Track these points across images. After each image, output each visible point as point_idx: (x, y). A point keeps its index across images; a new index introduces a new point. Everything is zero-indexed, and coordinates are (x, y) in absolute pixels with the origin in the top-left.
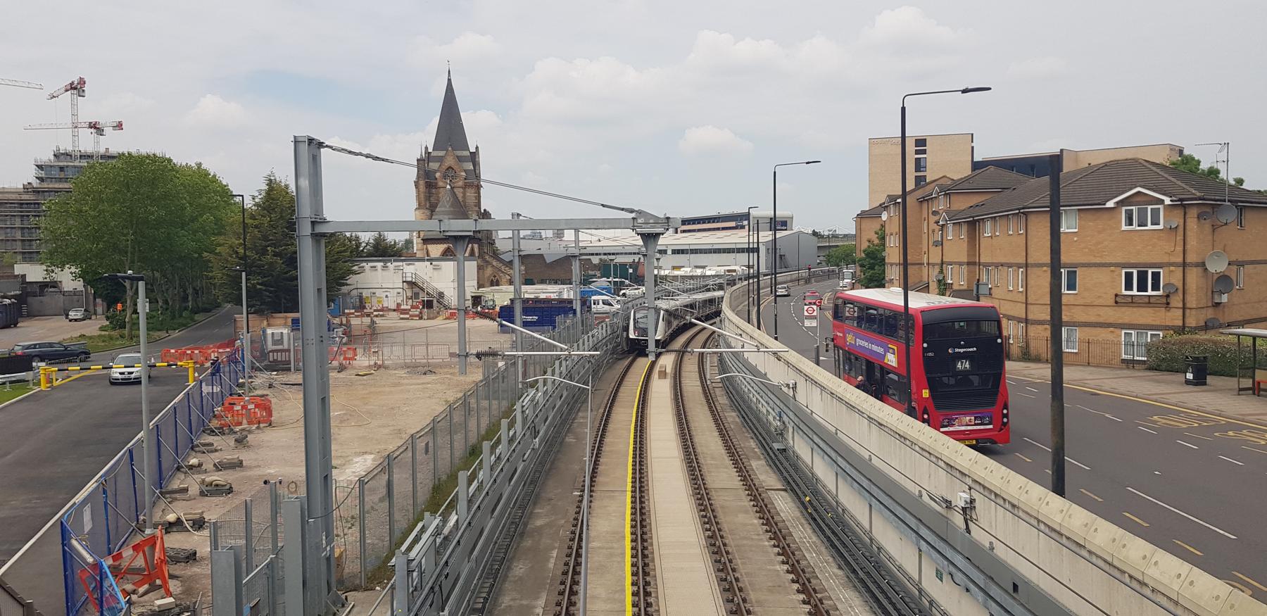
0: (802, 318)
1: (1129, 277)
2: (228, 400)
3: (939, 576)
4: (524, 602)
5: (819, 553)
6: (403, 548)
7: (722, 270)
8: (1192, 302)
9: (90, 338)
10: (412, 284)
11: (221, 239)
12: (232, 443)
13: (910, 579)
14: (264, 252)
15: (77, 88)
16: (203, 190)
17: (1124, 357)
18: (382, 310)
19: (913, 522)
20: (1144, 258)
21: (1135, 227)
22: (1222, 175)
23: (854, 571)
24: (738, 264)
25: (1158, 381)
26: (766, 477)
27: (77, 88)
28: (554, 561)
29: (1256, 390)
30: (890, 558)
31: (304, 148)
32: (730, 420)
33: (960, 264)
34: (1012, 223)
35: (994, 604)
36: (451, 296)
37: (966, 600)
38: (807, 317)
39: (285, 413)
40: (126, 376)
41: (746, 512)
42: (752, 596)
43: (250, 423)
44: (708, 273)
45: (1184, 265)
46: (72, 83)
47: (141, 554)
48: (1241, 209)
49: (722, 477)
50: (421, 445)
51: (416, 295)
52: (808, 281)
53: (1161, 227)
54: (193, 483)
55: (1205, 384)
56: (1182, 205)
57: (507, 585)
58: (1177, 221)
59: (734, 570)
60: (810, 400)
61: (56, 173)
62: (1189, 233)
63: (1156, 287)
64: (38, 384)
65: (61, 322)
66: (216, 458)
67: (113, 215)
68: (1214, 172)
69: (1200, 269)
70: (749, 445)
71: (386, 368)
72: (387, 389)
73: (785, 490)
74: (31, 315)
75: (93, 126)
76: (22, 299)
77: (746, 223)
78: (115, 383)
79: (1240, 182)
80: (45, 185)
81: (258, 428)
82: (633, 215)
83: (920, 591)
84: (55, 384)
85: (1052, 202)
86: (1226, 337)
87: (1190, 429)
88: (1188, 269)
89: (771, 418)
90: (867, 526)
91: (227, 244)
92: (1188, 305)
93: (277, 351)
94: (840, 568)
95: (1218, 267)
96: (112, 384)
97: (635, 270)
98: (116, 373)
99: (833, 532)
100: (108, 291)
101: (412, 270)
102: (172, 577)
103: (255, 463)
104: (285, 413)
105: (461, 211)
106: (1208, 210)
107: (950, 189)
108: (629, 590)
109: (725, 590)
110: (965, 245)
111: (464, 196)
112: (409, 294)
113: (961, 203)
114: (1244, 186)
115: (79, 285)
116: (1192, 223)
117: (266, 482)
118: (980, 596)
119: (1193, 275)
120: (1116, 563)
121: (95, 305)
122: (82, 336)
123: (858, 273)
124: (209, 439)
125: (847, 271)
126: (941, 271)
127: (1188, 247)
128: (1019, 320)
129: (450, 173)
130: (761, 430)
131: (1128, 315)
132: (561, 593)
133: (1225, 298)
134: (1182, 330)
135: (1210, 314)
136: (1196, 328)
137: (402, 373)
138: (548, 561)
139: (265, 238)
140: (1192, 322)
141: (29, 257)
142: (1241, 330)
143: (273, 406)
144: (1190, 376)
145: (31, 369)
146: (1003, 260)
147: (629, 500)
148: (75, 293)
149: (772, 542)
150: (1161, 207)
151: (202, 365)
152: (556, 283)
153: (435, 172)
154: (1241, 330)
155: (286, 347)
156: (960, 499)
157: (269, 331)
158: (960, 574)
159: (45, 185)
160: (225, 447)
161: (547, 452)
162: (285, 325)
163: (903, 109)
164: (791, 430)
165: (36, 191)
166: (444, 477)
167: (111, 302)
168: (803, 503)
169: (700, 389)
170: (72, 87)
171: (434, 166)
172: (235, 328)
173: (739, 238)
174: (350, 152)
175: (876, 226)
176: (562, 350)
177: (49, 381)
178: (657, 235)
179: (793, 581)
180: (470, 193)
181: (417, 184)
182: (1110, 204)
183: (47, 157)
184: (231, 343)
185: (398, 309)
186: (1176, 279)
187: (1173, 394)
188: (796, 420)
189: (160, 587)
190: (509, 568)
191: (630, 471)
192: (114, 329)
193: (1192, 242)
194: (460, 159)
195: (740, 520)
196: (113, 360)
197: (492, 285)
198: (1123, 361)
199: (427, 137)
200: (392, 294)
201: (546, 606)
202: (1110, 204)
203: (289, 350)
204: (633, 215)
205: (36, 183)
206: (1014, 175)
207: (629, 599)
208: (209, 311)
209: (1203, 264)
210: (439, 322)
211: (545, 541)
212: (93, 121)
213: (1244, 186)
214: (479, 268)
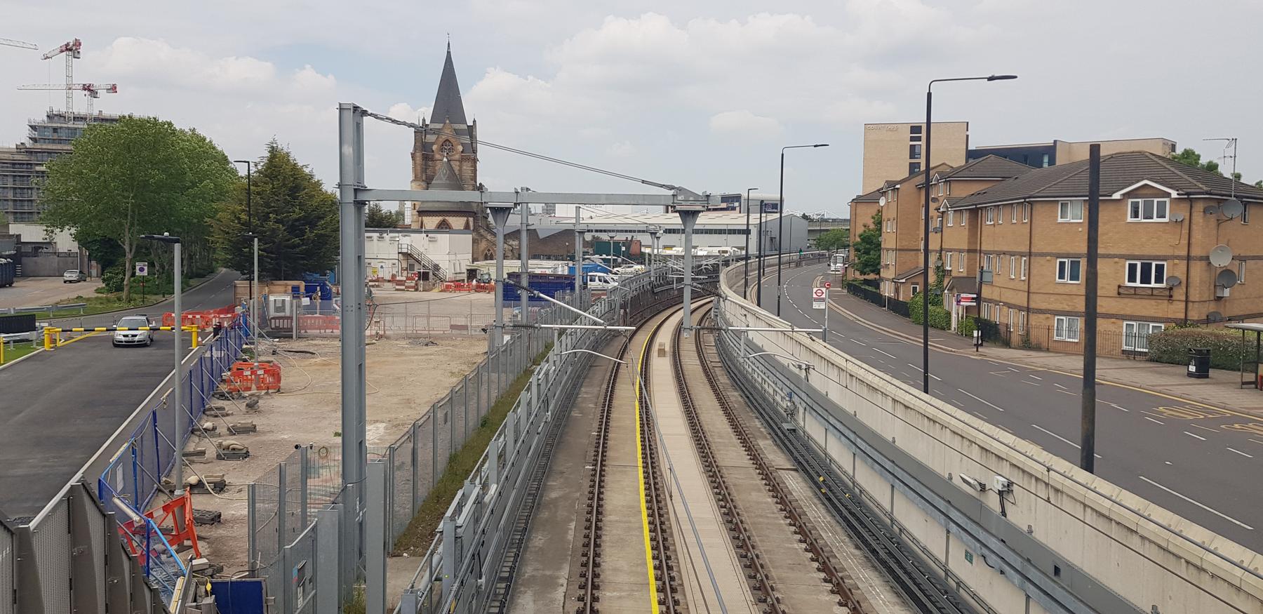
0: (811, 301)
1: (1132, 268)
2: (238, 364)
3: (969, 557)
4: (548, 573)
5: (835, 533)
6: (449, 513)
7: (715, 251)
8: (1195, 295)
9: (88, 299)
10: (408, 256)
11: (221, 205)
12: (243, 407)
13: (936, 560)
14: (266, 218)
15: (72, 49)
16: (202, 157)
17: (1125, 348)
18: (377, 280)
19: (942, 505)
20: (1147, 251)
21: (1141, 219)
22: (1220, 169)
23: (874, 551)
24: (730, 246)
25: (1160, 373)
26: (775, 457)
27: (72, 49)
28: (573, 532)
29: (1262, 384)
30: (914, 539)
31: (349, 115)
32: (733, 399)
33: (960, 251)
34: (1017, 211)
35: (1032, 587)
36: (447, 270)
37: (998, 580)
38: (816, 300)
39: (291, 379)
40: (130, 339)
41: (759, 490)
42: (774, 573)
43: (259, 388)
44: (700, 253)
45: (1188, 258)
46: (67, 45)
47: (171, 515)
48: (1245, 204)
49: (731, 455)
50: (440, 415)
51: (411, 267)
52: (798, 264)
53: (1166, 220)
54: (210, 447)
55: (1207, 377)
56: (1188, 199)
57: (528, 555)
58: (1183, 214)
59: (753, 547)
60: (825, 383)
61: (49, 134)
62: (1194, 227)
63: (1159, 279)
64: (42, 343)
65: (57, 283)
66: (230, 421)
67: (115, 177)
68: (1212, 167)
69: (1204, 263)
70: (755, 424)
71: (388, 338)
72: (391, 359)
73: (796, 470)
74: (25, 275)
75: (87, 88)
76: (17, 258)
77: (736, 204)
78: (118, 345)
79: (1238, 176)
80: (38, 146)
81: (267, 393)
82: (672, 192)
83: (947, 572)
84: (59, 344)
85: (1091, 192)
86: (1230, 332)
87: (1197, 421)
88: (1192, 263)
89: (778, 398)
90: (888, 508)
91: (227, 212)
92: (1191, 298)
93: (279, 318)
94: (857, 547)
95: (1222, 261)
96: (116, 346)
97: (628, 248)
98: (119, 335)
99: (851, 513)
100: (103, 253)
101: (408, 242)
102: (200, 538)
103: (268, 429)
104: (291, 379)
105: (457, 182)
106: (1215, 204)
107: (950, 177)
108: (651, 564)
109: (746, 566)
110: (966, 232)
111: (460, 170)
112: (405, 265)
113: (962, 191)
114: (1242, 181)
115: (74, 247)
116: (1198, 217)
117: (297, 447)
118: (1017, 578)
119: (1197, 269)
120: (1171, 548)
121: (90, 267)
122: (79, 298)
123: (852, 257)
124: (220, 403)
125: (841, 255)
126: (940, 258)
127: (1193, 240)
128: (1020, 309)
129: (447, 145)
130: (767, 409)
131: (1130, 306)
132: (585, 565)
133: (1227, 293)
134: (1184, 323)
135: (1212, 307)
136: (1198, 321)
137: (403, 343)
138: (567, 533)
139: (267, 205)
140: (1194, 315)
141: (21, 217)
142: (1241, 325)
143: (282, 373)
144: (1192, 368)
145: (34, 329)
146: (1005, 249)
147: (641, 475)
148: (69, 254)
149: (788, 521)
150: (1167, 200)
151: (203, 329)
152: (549, 258)
153: (433, 144)
154: (1241, 325)
155: (288, 314)
156: (997, 483)
157: (272, 298)
158: (993, 556)
159: (38, 146)
160: (236, 412)
161: (557, 426)
162: (285, 292)
163: (929, 95)
164: (801, 410)
165: (30, 152)
166: (460, 447)
167: (106, 264)
168: (816, 483)
169: (700, 368)
170: (67, 48)
171: (431, 138)
172: (235, 294)
173: (735, 219)
174: (394, 121)
175: (872, 210)
176: (595, 323)
177: (53, 341)
178: (695, 214)
179: (812, 560)
180: (467, 167)
181: (413, 156)
182: (1117, 196)
183: (41, 118)
184: (231, 309)
185: (393, 280)
186: (1180, 272)
187: (1173, 384)
188: (809, 401)
189: (190, 547)
190: (529, 539)
191: (639, 447)
192: (110, 291)
193: (1197, 236)
194: (458, 132)
195: (754, 499)
196: (115, 322)
197: (486, 258)
198: (1124, 352)
199: (424, 112)
200: (387, 264)
201: (570, 576)
202: (1117, 196)
203: (291, 318)
204: (672, 192)
205: (29, 144)
206: (1015, 165)
207: (651, 573)
208: (204, 276)
209: (1207, 258)
210: (434, 294)
211: (561, 513)
212: (87, 83)
213: (1242, 181)
214: (474, 241)
